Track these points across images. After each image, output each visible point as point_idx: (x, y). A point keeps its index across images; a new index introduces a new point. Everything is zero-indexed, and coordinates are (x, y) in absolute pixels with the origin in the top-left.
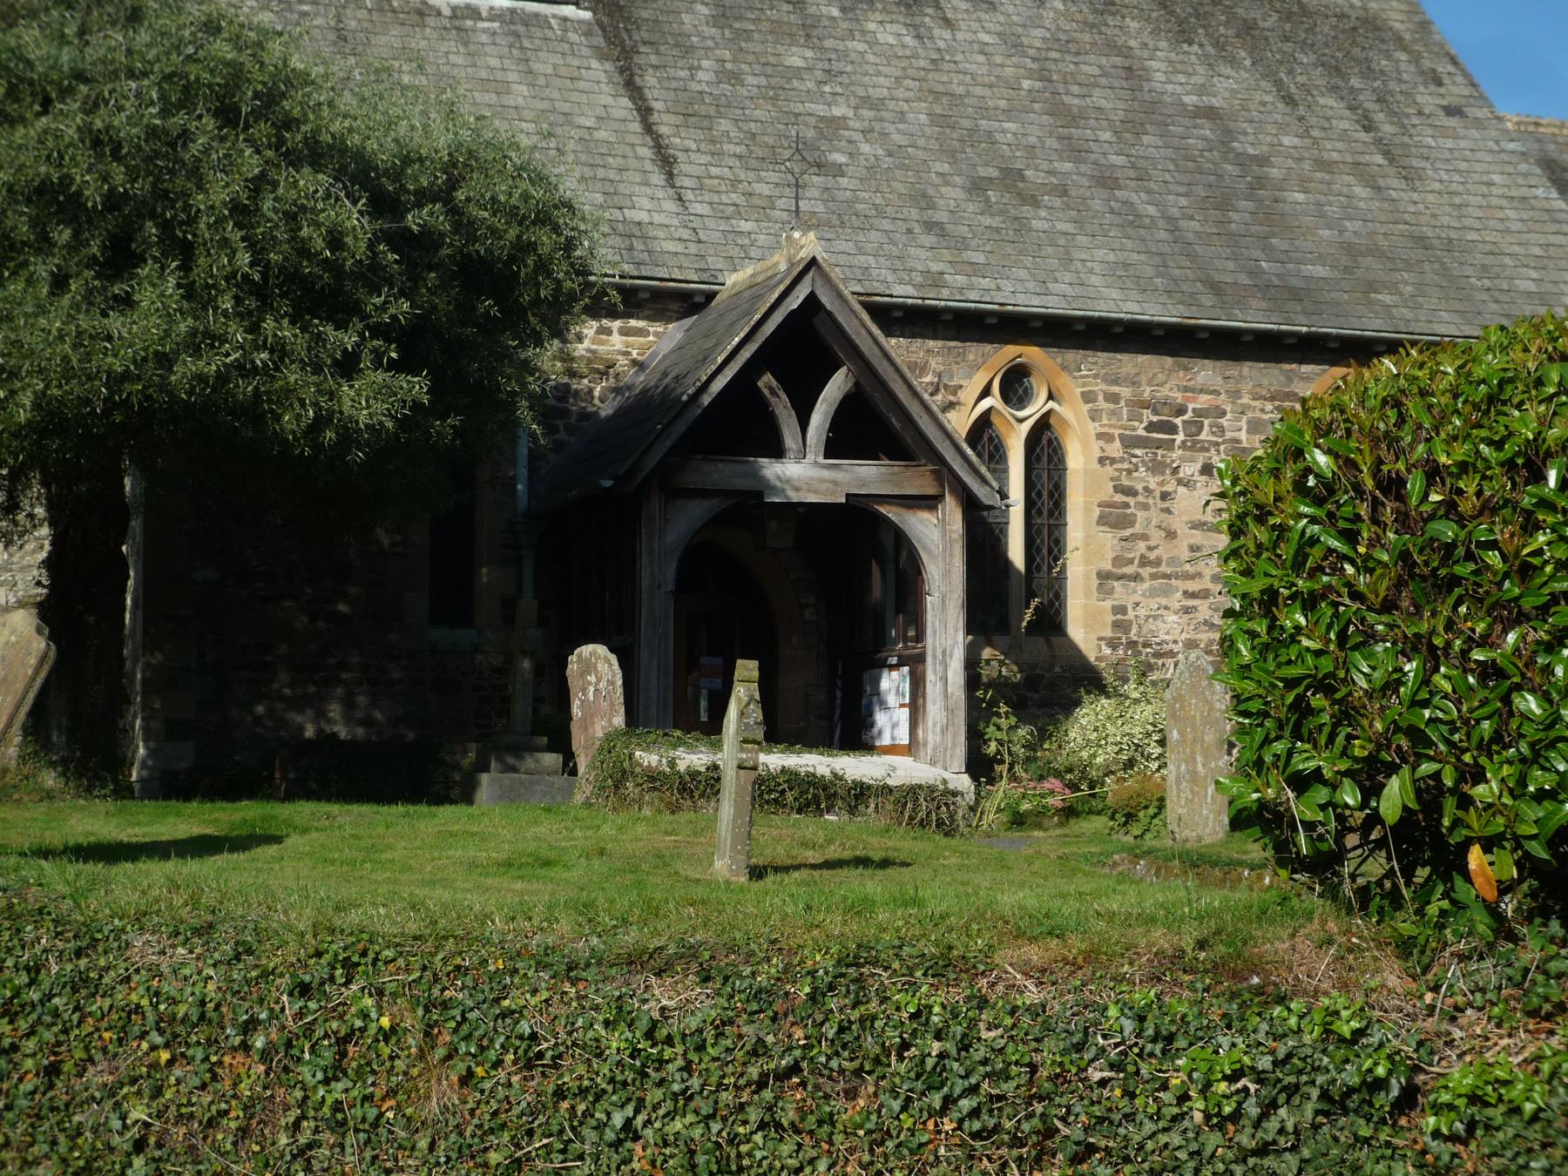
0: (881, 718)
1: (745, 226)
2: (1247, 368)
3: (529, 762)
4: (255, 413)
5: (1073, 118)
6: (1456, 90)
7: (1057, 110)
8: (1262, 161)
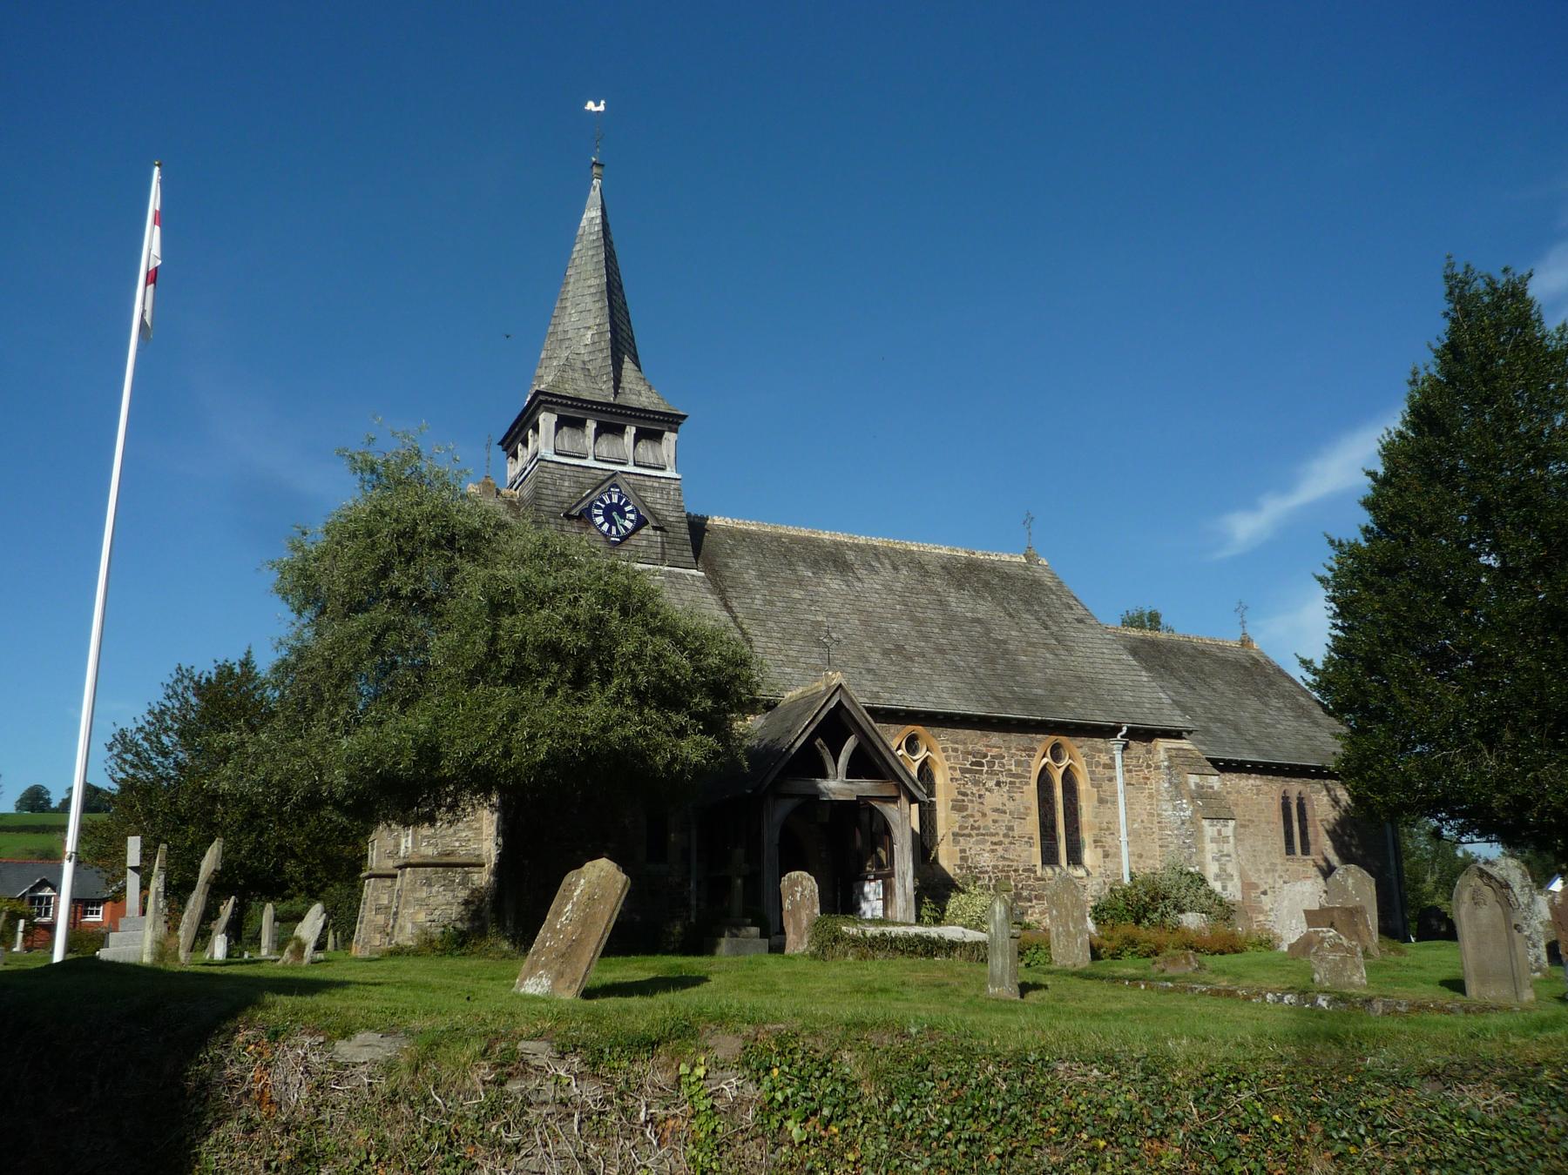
0: (864, 906)
1: (789, 670)
2: (1013, 736)
3: (744, 932)
4: (641, 756)
5: (921, 623)
6: (1080, 612)
7: (913, 619)
8: (1005, 642)
